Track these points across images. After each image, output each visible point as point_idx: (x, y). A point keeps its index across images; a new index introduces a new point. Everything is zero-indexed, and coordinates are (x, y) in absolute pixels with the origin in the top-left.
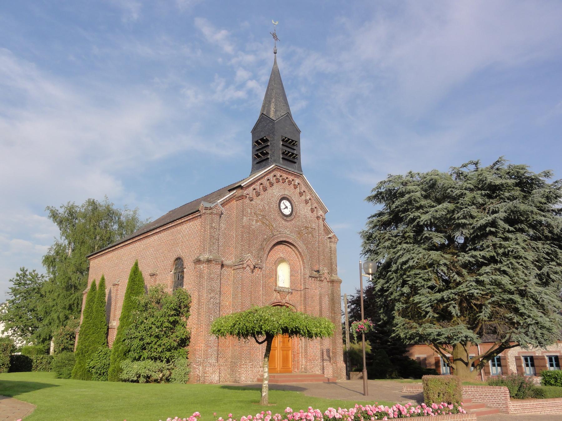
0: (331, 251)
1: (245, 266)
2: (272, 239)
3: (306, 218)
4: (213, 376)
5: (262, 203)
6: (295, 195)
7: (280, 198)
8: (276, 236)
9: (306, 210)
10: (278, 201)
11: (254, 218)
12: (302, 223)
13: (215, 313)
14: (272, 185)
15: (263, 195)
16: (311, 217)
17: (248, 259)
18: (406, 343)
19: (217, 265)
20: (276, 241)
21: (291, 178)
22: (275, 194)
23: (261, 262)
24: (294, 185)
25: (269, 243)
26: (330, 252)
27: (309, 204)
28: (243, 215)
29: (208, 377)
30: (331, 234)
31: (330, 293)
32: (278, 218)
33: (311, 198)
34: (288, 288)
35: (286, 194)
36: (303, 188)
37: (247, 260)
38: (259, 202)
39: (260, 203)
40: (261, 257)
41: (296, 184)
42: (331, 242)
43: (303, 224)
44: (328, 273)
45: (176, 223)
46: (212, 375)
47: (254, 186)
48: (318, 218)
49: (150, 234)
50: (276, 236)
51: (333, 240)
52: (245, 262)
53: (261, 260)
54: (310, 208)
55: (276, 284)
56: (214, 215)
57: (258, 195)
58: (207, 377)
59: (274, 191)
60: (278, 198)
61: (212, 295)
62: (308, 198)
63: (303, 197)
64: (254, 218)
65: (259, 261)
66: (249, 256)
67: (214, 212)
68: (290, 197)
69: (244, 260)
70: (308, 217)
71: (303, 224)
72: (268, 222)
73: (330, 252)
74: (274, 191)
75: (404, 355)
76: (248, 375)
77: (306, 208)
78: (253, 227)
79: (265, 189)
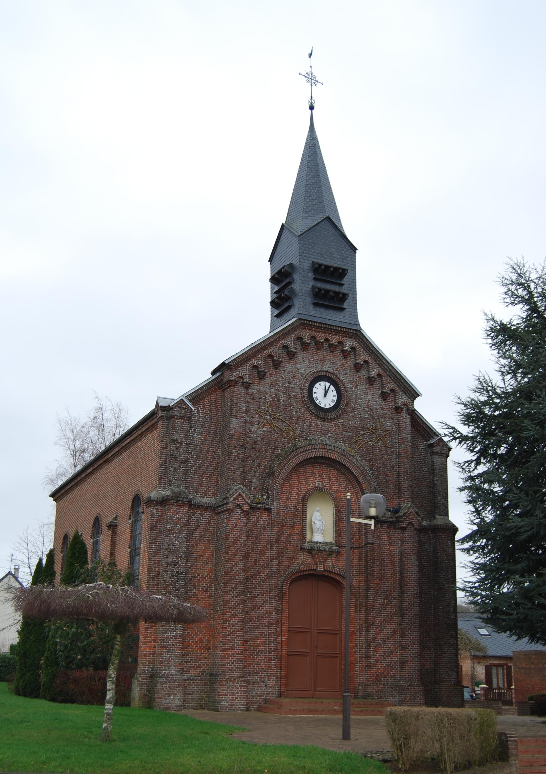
0: (433, 470)
1: (231, 506)
2: (292, 455)
3: (370, 410)
4: (172, 698)
5: (272, 390)
6: (346, 369)
7: (310, 379)
8: (301, 450)
9: (370, 397)
10: (307, 385)
11: (256, 420)
12: (362, 420)
13: (176, 590)
14: (291, 355)
15: (273, 376)
16: (382, 409)
17: (237, 494)
18: (517, 630)
19: (181, 506)
20: (301, 458)
21: (334, 340)
22: (302, 371)
23: (268, 498)
24: (343, 352)
25: (285, 462)
26: (431, 472)
27: (377, 384)
28: (232, 415)
29: (161, 698)
30: (435, 437)
31: (432, 549)
32: (308, 415)
33: (382, 372)
34: (331, 544)
35: (325, 369)
36: (363, 356)
37: (234, 496)
38: (265, 389)
39: (267, 391)
40: (268, 490)
41: (347, 348)
42: (433, 453)
43: (363, 422)
44: (417, 513)
45: (135, 436)
46: (169, 696)
47: (254, 361)
48: (398, 410)
49: (110, 455)
50: (301, 450)
51: (437, 449)
52: (232, 499)
53: (268, 494)
54: (380, 392)
55: (304, 538)
56: (176, 419)
57: (261, 376)
58: (159, 698)
59: (298, 366)
60: (307, 380)
61: (170, 559)
62: (374, 373)
63: (363, 373)
64: (256, 420)
65: (265, 497)
66: (240, 488)
67: (176, 413)
68: (333, 374)
69: (228, 496)
70: (376, 409)
71: (363, 422)
72: (285, 424)
73: (431, 472)
74: (298, 366)
75: (44, 566)
76: (236, 698)
77: (370, 392)
78: (252, 435)
79: (277, 365)
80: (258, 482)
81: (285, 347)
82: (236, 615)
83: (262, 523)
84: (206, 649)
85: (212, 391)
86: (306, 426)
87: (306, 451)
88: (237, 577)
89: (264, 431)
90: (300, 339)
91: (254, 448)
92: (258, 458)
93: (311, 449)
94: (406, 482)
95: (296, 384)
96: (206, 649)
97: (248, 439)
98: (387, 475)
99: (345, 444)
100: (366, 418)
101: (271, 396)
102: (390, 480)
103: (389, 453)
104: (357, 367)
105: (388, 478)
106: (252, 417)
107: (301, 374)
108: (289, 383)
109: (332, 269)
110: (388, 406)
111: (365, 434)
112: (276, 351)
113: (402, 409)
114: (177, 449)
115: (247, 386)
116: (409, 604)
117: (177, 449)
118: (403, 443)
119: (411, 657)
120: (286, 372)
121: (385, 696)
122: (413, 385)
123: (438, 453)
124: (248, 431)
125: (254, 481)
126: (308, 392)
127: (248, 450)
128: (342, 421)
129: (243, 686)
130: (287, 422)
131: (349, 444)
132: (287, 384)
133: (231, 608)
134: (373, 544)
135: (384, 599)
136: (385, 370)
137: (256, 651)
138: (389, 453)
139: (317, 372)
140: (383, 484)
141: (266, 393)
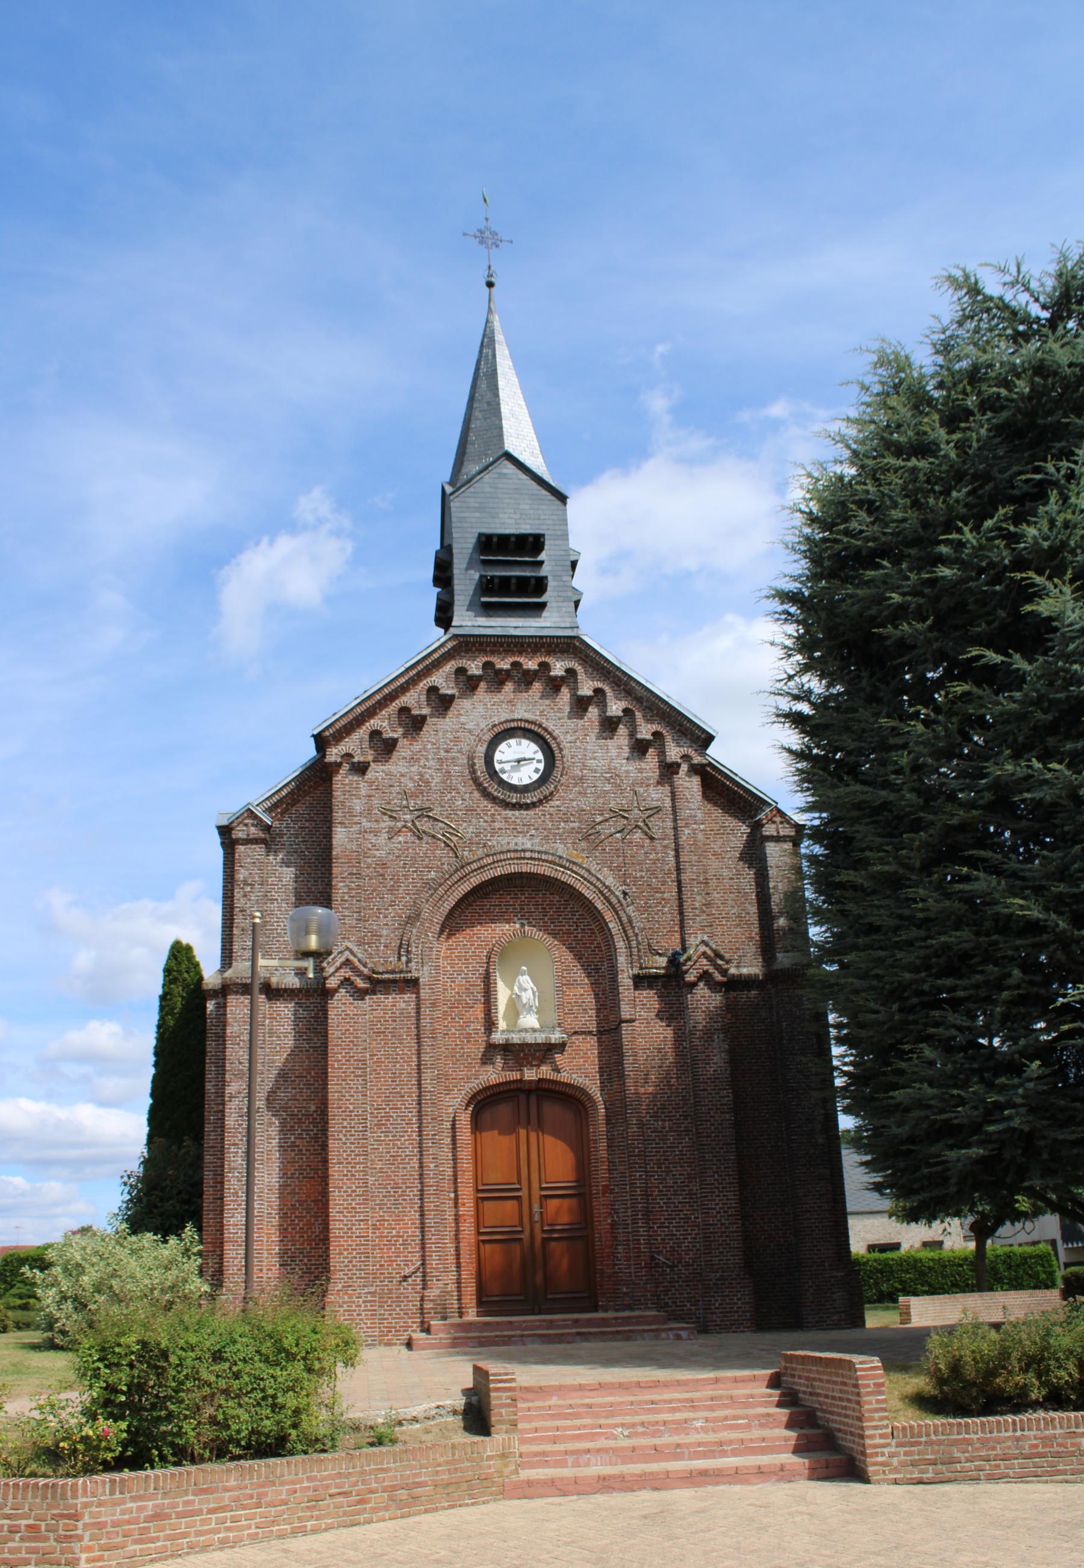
7: (488, 737)
8: (474, 866)
11: (383, 825)
39: (403, 770)
43: (601, 800)
47: (374, 723)
56: (242, 844)
59: (463, 719)
64: (383, 825)
71: (601, 800)
74: (463, 719)
78: (377, 853)
80: (392, 935)
81: (433, 690)
82: (353, 1175)
83: (403, 1005)
84: (320, 1240)
85: (311, 787)
86: (485, 821)
87: (483, 867)
88: (351, 1107)
89: (400, 843)
90: (461, 671)
91: (383, 875)
92: (391, 891)
93: (494, 863)
94: (698, 898)
95: (460, 751)
96: (320, 1240)
97: (369, 860)
98: (658, 890)
99: (565, 844)
100: (607, 792)
101: (411, 779)
102: (664, 899)
103: (659, 848)
104: (581, 705)
105: (658, 895)
106: (376, 821)
107: (470, 732)
108: (447, 751)
109: (531, 539)
110: (651, 762)
111: (606, 820)
112: (414, 699)
113: (679, 765)
114: (245, 896)
115: (361, 769)
116: (712, 1125)
117: (245, 896)
118: (687, 825)
119: (722, 1224)
120: (440, 734)
121: (675, 1303)
122: (696, 716)
123: (772, 837)
124: (370, 846)
125: (384, 932)
126: (486, 762)
127: (371, 879)
128: (558, 803)
129: (370, 1301)
130: (446, 821)
131: (574, 843)
132: (443, 754)
133: (341, 1163)
134: (633, 1021)
135: (664, 1121)
136: (638, 700)
137: (402, 1236)
138: (659, 848)
139: (501, 723)
140: (650, 907)
141: (402, 775)
